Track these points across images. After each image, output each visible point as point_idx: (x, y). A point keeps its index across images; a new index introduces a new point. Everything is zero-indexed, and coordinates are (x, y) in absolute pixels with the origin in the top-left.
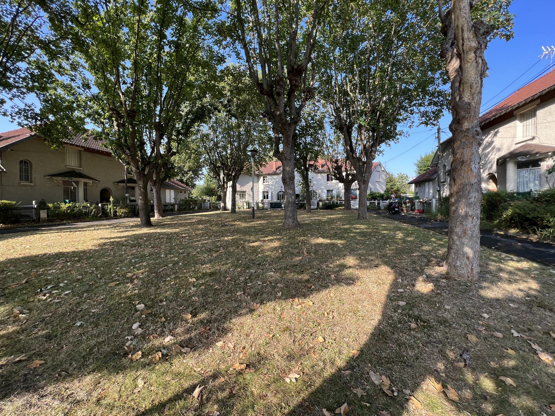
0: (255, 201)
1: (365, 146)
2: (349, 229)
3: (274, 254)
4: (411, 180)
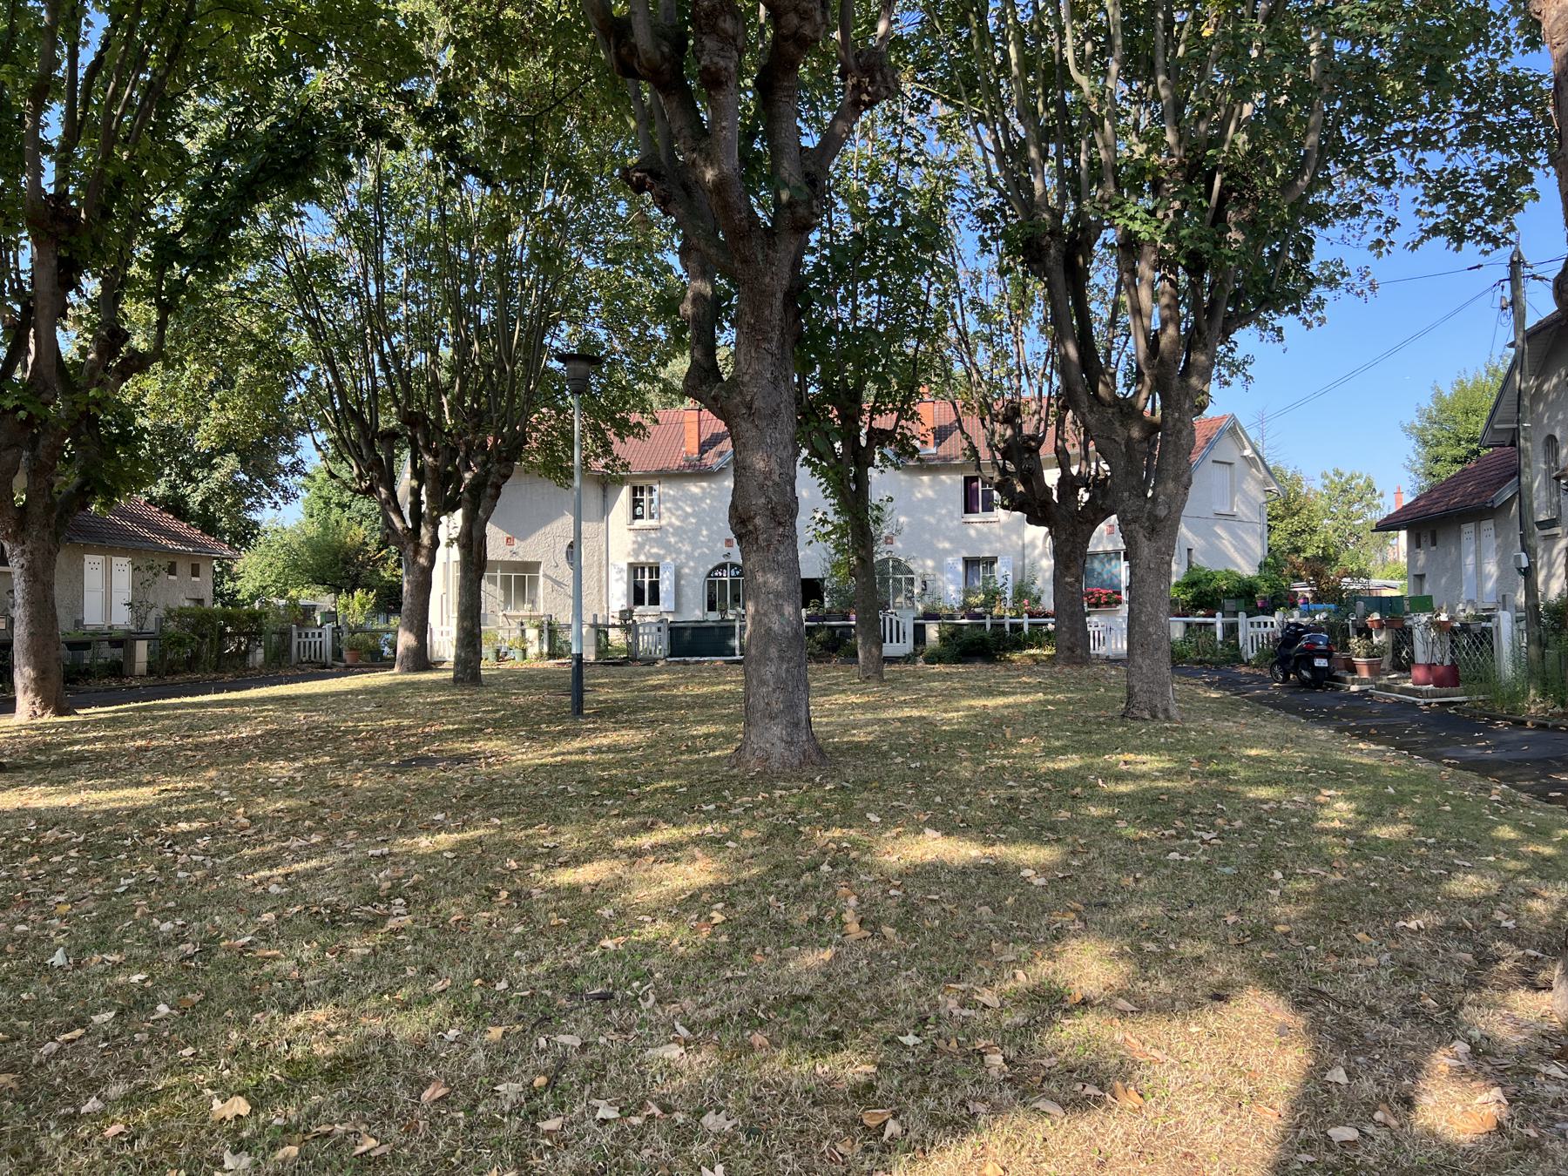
0: (588, 618)
1: (1153, 343)
2: (1078, 776)
3: (683, 938)
4: (1389, 506)
